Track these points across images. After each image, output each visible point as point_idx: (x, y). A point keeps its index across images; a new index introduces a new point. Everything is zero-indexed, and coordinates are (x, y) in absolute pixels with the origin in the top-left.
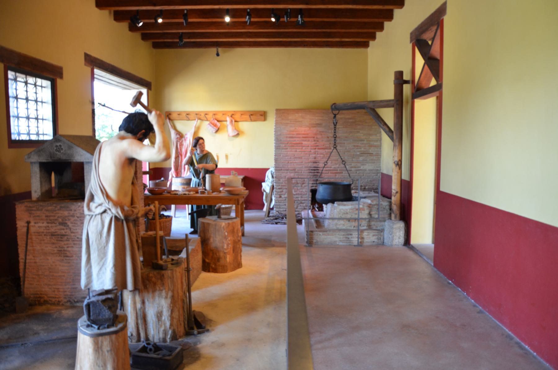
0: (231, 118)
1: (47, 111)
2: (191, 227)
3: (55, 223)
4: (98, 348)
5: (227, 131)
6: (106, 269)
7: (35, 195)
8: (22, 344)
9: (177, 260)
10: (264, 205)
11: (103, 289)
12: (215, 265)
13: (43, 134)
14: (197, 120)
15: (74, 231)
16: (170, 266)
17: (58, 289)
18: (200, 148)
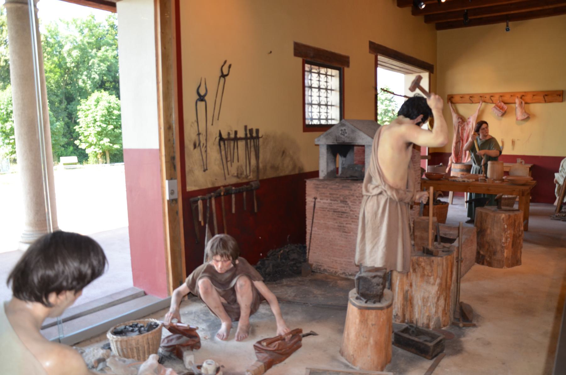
0: (520, 100)
1: (334, 98)
2: (469, 216)
3: (337, 201)
4: (364, 321)
5: (516, 114)
6: (378, 248)
7: (322, 175)
8: (304, 303)
9: (449, 248)
10: (555, 198)
11: (373, 267)
12: (490, 258)
13: (332, 119)
14: (481, 103)
15: (354, 210)
16: (440, 253)
17: (336, 260)
18: (482, 132)
